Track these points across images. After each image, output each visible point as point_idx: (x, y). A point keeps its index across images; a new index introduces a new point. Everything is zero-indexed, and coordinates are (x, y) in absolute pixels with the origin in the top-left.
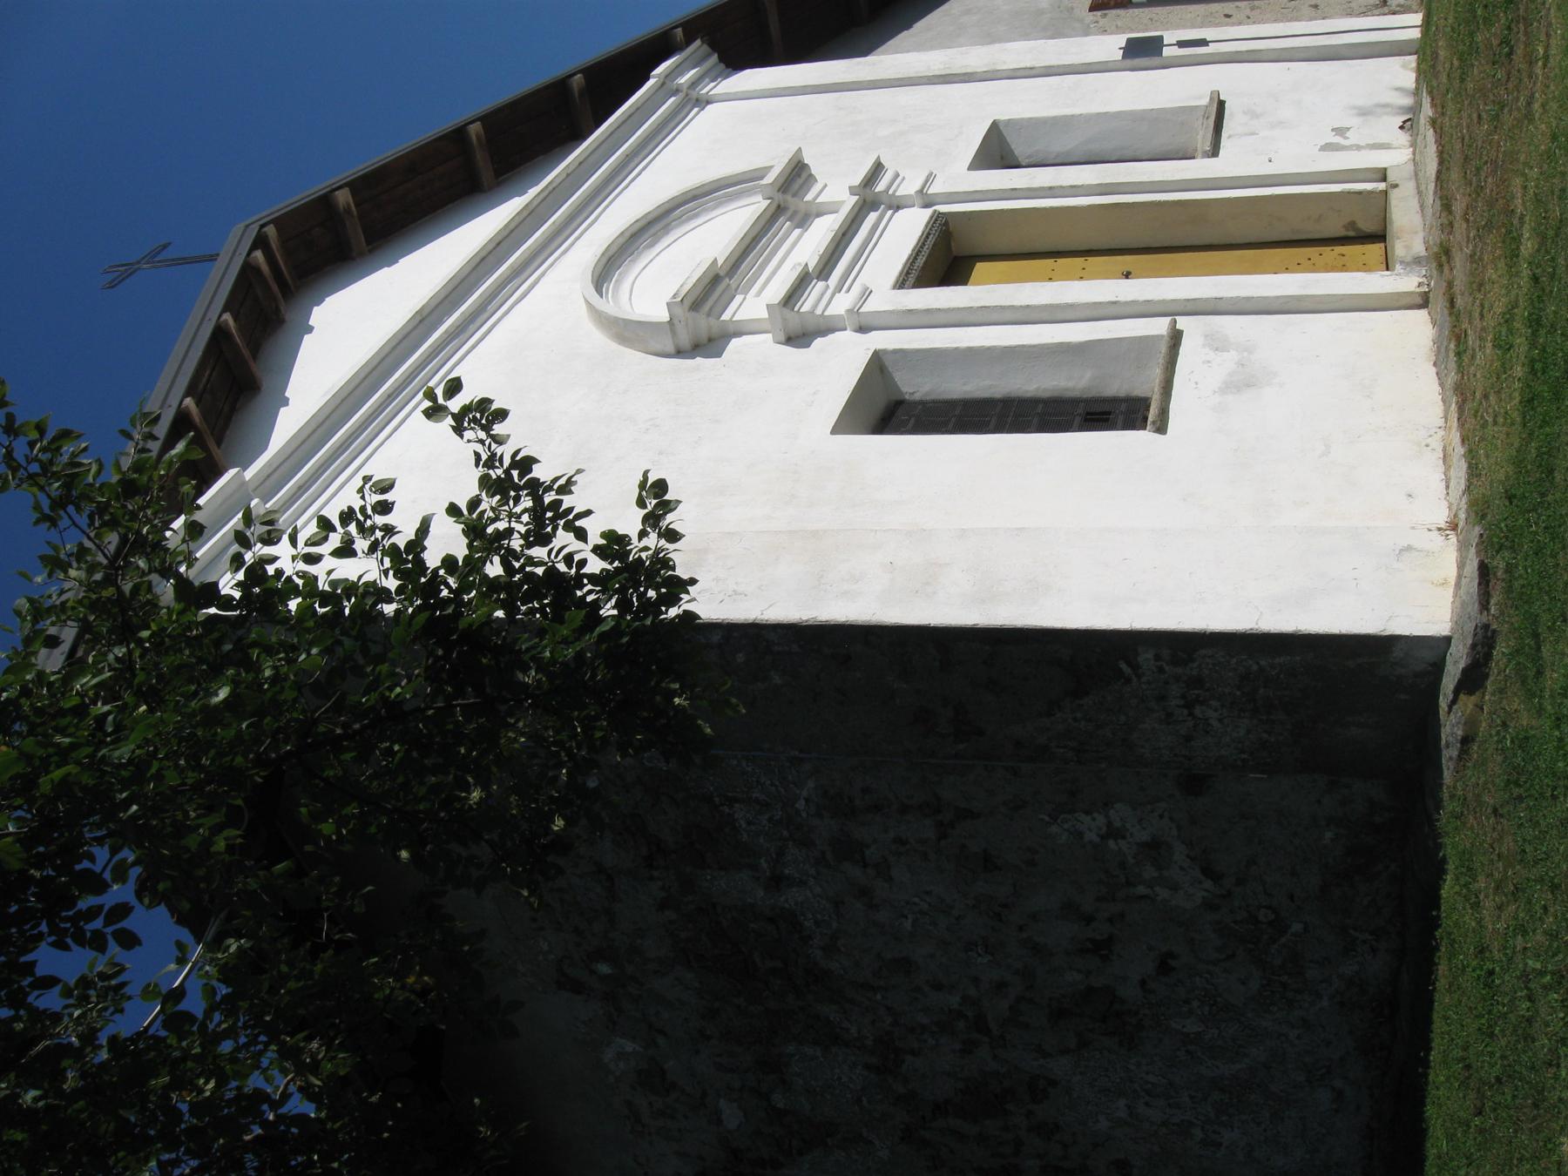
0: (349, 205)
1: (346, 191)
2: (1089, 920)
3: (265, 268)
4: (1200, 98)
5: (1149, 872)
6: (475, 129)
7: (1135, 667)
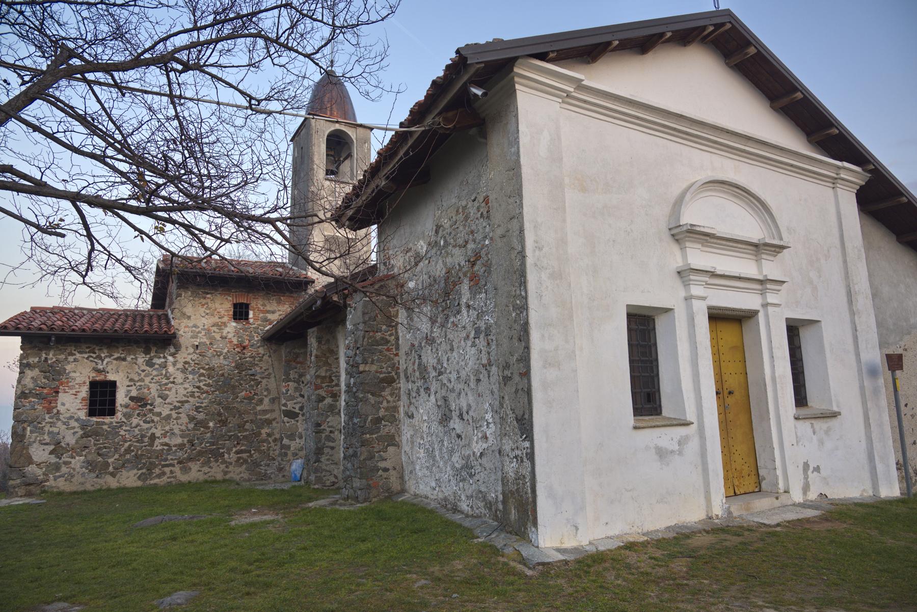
0: (748, 54)
1: (756, 51)
2: (467, 413)
3: (706, 33)
4: (838, 406)
5: (480, 435)
6: (799, 95)
7: (524, 440)
